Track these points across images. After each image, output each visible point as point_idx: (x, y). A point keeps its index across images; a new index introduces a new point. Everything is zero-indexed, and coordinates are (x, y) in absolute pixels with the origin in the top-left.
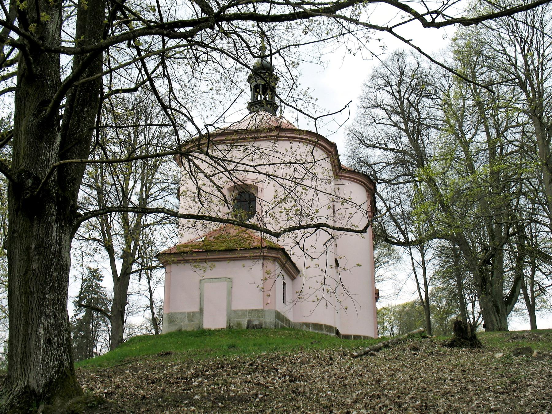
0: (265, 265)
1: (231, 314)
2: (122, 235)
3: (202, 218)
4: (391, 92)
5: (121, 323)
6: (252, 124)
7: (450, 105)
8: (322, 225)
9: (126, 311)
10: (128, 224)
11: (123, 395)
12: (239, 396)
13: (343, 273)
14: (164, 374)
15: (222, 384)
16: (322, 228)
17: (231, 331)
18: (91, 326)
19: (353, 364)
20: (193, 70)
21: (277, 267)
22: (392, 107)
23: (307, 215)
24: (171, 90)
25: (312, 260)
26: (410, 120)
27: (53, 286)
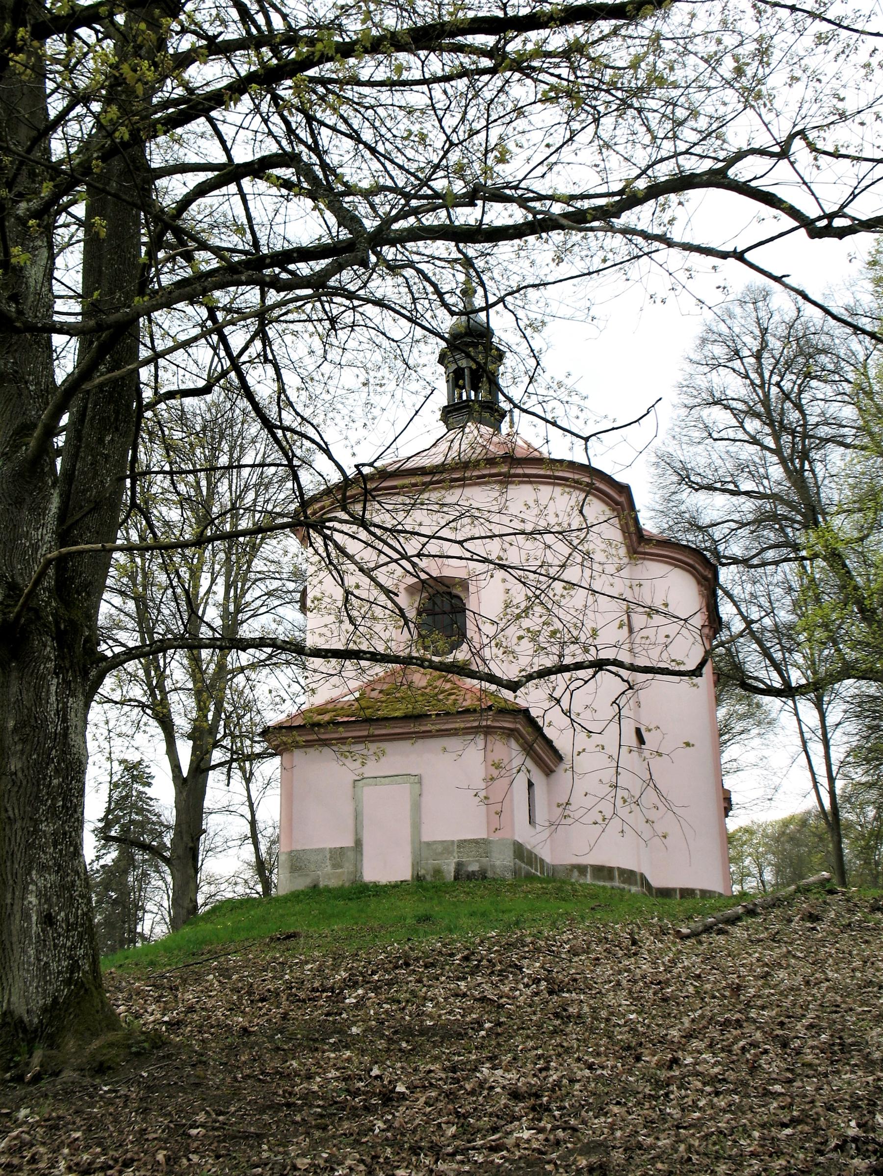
0: (489, 747)
2: (189, 690)
3: (357, 655)
4: (743, 371)
5: (192, 871)
6: (453, 454)
7: (870, 394)
8: (607, 662)
9: (201, 848)
10: (200, 669)
11: (201, 1026)
12: (443, 1027)
13: (656, 764)
14: (286, 982)
15: (407, 1001)
16: (608, 667)
17: (421, 887)
18: (130, 879)
19: (680, 952)
20: (325, 344)
21: (514, 753)
22: (746, 403)
23: (576, 641)
24: (282, 390)
25: (589, 737)
26: (786, 429)
27: (53, 805)
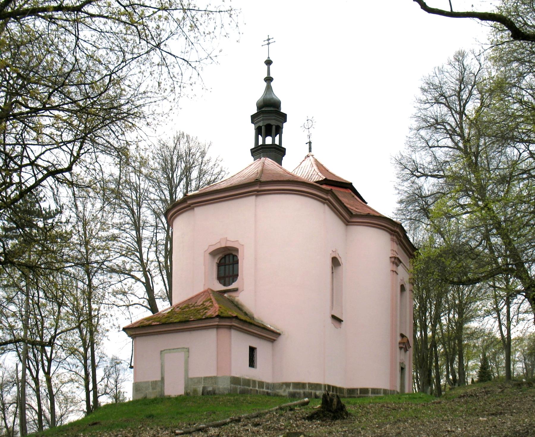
1: (188, 381)
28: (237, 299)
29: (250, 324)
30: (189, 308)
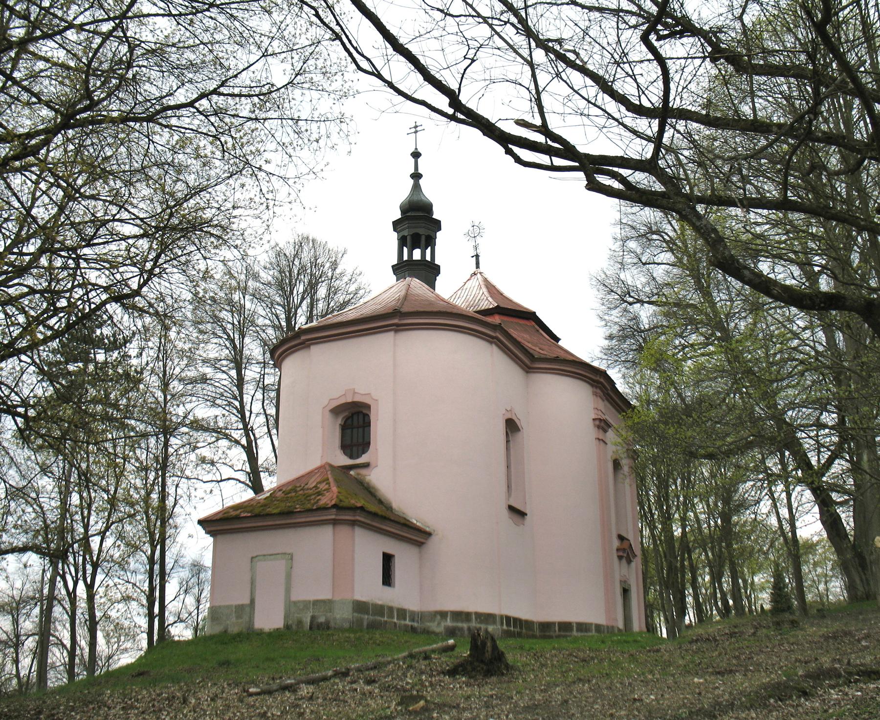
1: (291, 606)
28: (368, 478)
29: (384, 518)
30: (296, 491)
